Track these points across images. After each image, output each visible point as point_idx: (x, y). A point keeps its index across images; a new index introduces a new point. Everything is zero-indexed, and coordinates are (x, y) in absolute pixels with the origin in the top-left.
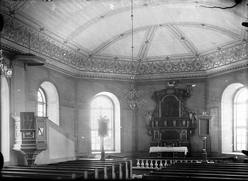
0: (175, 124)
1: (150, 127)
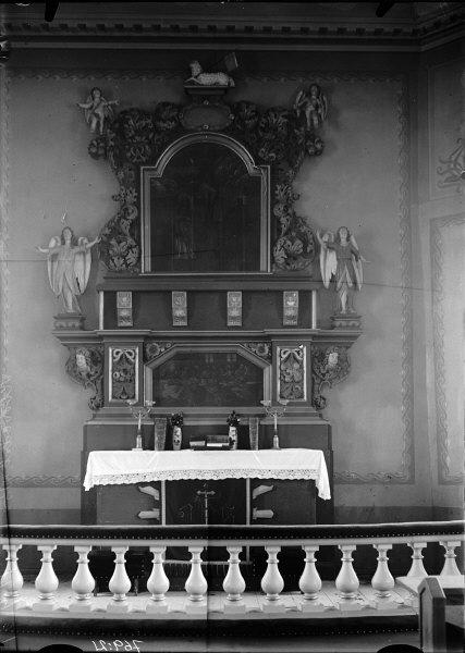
0: (124, 313)
1: (82, 328)
